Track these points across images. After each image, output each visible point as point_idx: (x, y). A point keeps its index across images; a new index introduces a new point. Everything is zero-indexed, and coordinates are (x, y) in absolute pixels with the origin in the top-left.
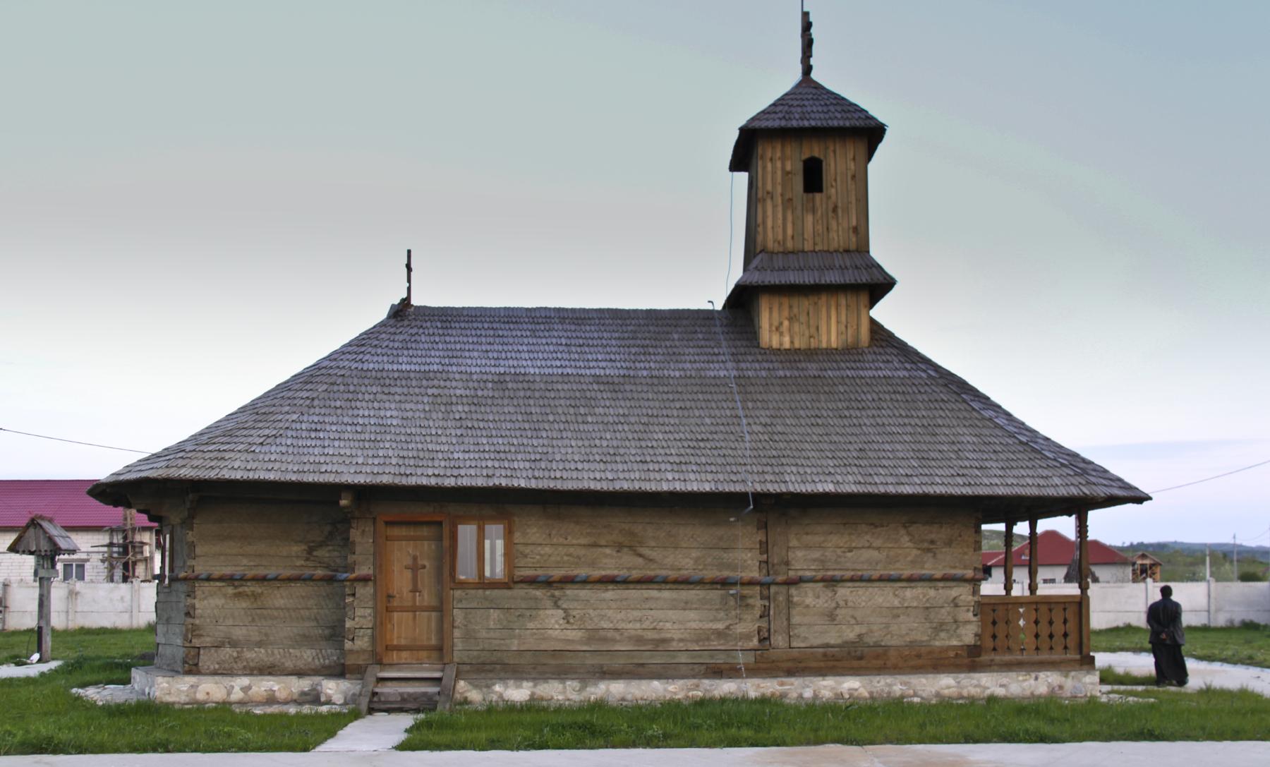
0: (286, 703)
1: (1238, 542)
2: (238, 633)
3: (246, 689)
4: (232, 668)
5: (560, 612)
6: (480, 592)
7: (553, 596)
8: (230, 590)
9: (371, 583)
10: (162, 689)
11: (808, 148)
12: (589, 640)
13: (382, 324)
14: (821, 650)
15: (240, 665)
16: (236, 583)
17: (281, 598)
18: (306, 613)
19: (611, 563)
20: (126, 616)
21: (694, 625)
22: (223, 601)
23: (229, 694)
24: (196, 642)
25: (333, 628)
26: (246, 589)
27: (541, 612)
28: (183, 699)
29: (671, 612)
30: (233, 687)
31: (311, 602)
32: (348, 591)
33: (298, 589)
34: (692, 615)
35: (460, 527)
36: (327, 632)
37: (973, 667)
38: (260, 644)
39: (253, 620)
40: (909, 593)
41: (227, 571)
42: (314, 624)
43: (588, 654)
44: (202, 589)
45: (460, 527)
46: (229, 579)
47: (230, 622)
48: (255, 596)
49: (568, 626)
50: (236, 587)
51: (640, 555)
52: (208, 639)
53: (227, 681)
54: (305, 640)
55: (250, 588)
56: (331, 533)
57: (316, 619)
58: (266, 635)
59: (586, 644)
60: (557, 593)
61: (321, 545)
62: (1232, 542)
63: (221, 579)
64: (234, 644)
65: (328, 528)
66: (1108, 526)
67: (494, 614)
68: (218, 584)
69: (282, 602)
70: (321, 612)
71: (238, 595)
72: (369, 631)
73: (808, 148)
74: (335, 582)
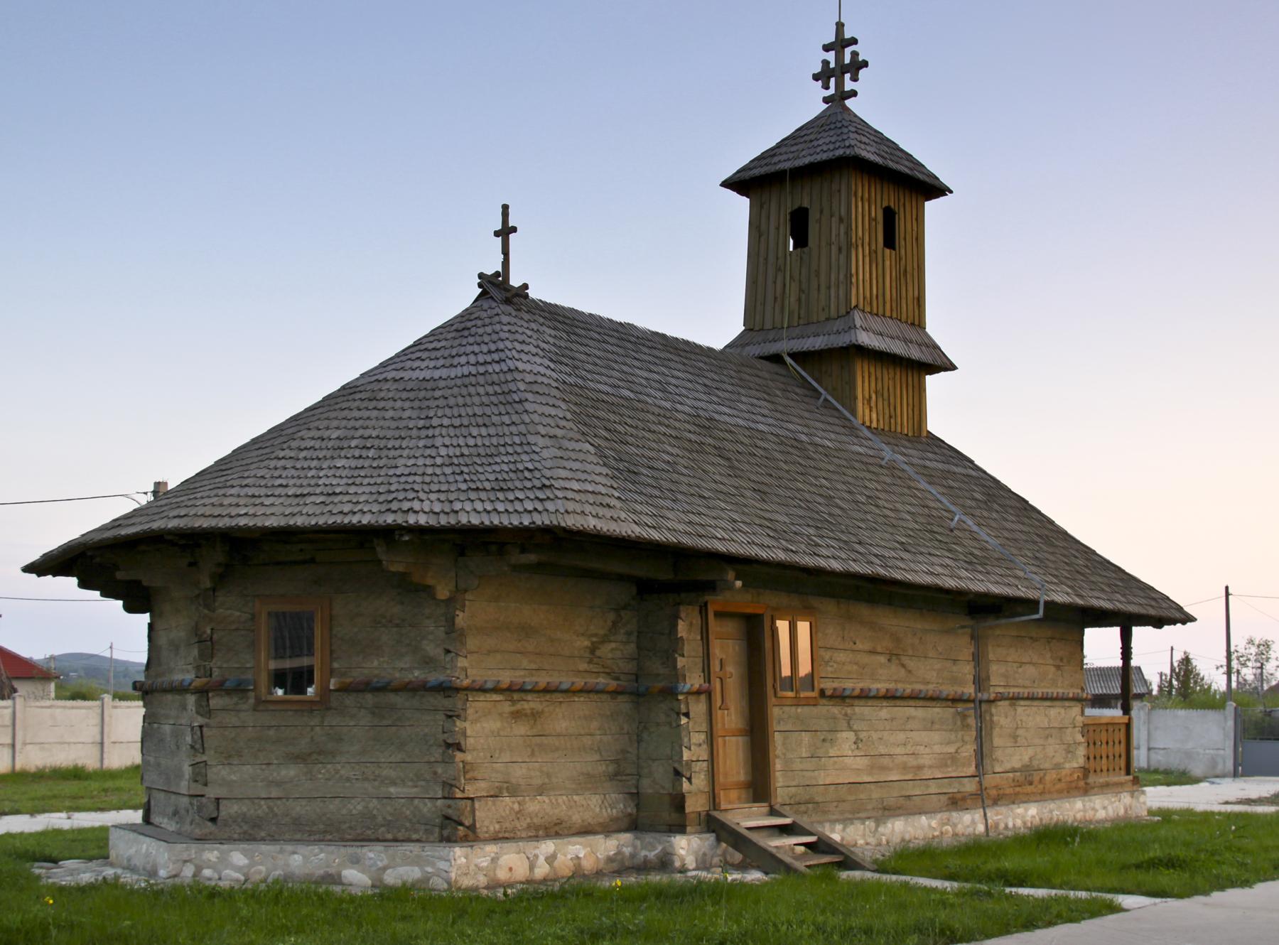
0: (881, 868)
1: (117, 655)
2: (519, 773)
3: (551, 859)
4: (514, 830)
5: (852, 733)
6: (793, 709)
7: (846, 715)
8: (507, 708)
9: (703, 697)
10: (459, 868)
11: (836, 204)
12: (871, 769)
13: (466, 315)
14: (1011, 775)
15: (524, 823)
16: (516, 696)
17: (565, 719)
18: (587, 741)
19: (884, 678)
20: (95, 751)
21: (937, 749)
22: (498, 724)
23: (532, 868)
24: (212, 792)
25: (616, 762)
26: (526, 706)
27: (839, 735)
28: (482, 880)
29: (924, 733)
30: (536, 856)
31: (595, 724)
32: (683, 709)
33: (582, 705)
34: (936, 736)
35: (1134, 629)
36: (611, 768)
37: (1086, 790)
38: (541, 790)
39: (533, 754)
40: (1053, 712)
41: (506, 678)
42: (597, 757)
43: (872, 786)
44: (477, 704)
45: (1134, 629)
46: (512, 691)
47: (506, 757)
48: (535, 715)
49: (857, 753)
50: (513, 702)
51: (903, 666)
52: (483, 785)
53: (531, 848)
54: (587, 783)
55: (532, 703)
56: (614, 623)
57: (599, 750)
58: (548, 775)
59: (870, 774)
60: (849, 710)
61: (605, 640)
62: (107, 654)
63: (496, 690)
64: (513, 791)
65: (611, 616)
66: (1154, 651)
67: (806, 737)
68: (496, 697)
69: (564, 724)
70: (605, 738)
71: (517, 715)
72: (705, 764)
73: (836, 204)
74: (647, 694)
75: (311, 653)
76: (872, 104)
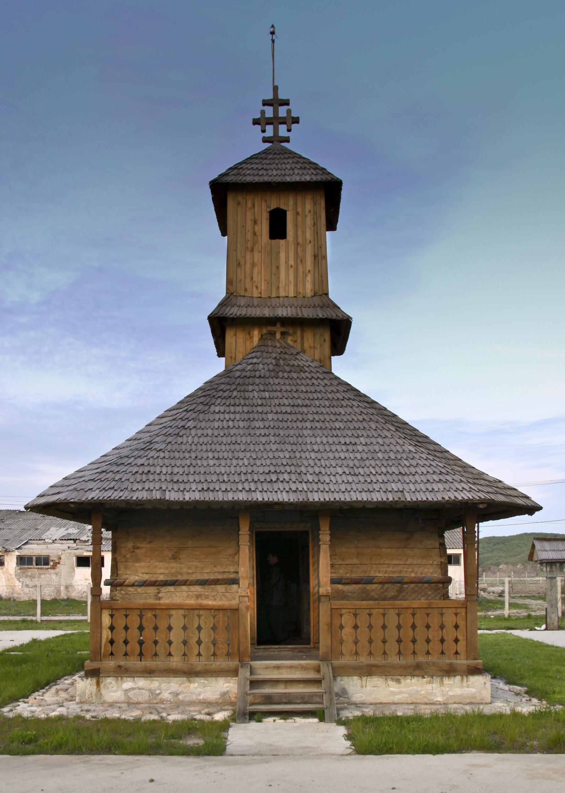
75: (86, 615)
76: (299, 142)
